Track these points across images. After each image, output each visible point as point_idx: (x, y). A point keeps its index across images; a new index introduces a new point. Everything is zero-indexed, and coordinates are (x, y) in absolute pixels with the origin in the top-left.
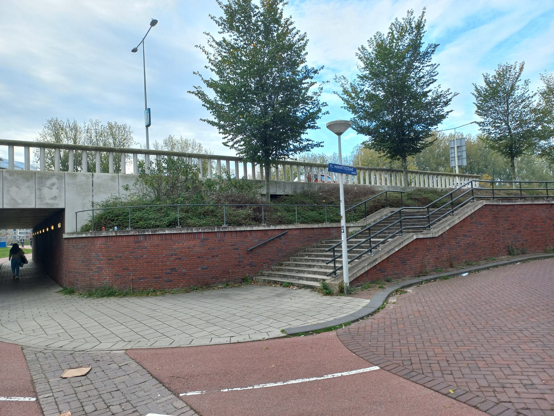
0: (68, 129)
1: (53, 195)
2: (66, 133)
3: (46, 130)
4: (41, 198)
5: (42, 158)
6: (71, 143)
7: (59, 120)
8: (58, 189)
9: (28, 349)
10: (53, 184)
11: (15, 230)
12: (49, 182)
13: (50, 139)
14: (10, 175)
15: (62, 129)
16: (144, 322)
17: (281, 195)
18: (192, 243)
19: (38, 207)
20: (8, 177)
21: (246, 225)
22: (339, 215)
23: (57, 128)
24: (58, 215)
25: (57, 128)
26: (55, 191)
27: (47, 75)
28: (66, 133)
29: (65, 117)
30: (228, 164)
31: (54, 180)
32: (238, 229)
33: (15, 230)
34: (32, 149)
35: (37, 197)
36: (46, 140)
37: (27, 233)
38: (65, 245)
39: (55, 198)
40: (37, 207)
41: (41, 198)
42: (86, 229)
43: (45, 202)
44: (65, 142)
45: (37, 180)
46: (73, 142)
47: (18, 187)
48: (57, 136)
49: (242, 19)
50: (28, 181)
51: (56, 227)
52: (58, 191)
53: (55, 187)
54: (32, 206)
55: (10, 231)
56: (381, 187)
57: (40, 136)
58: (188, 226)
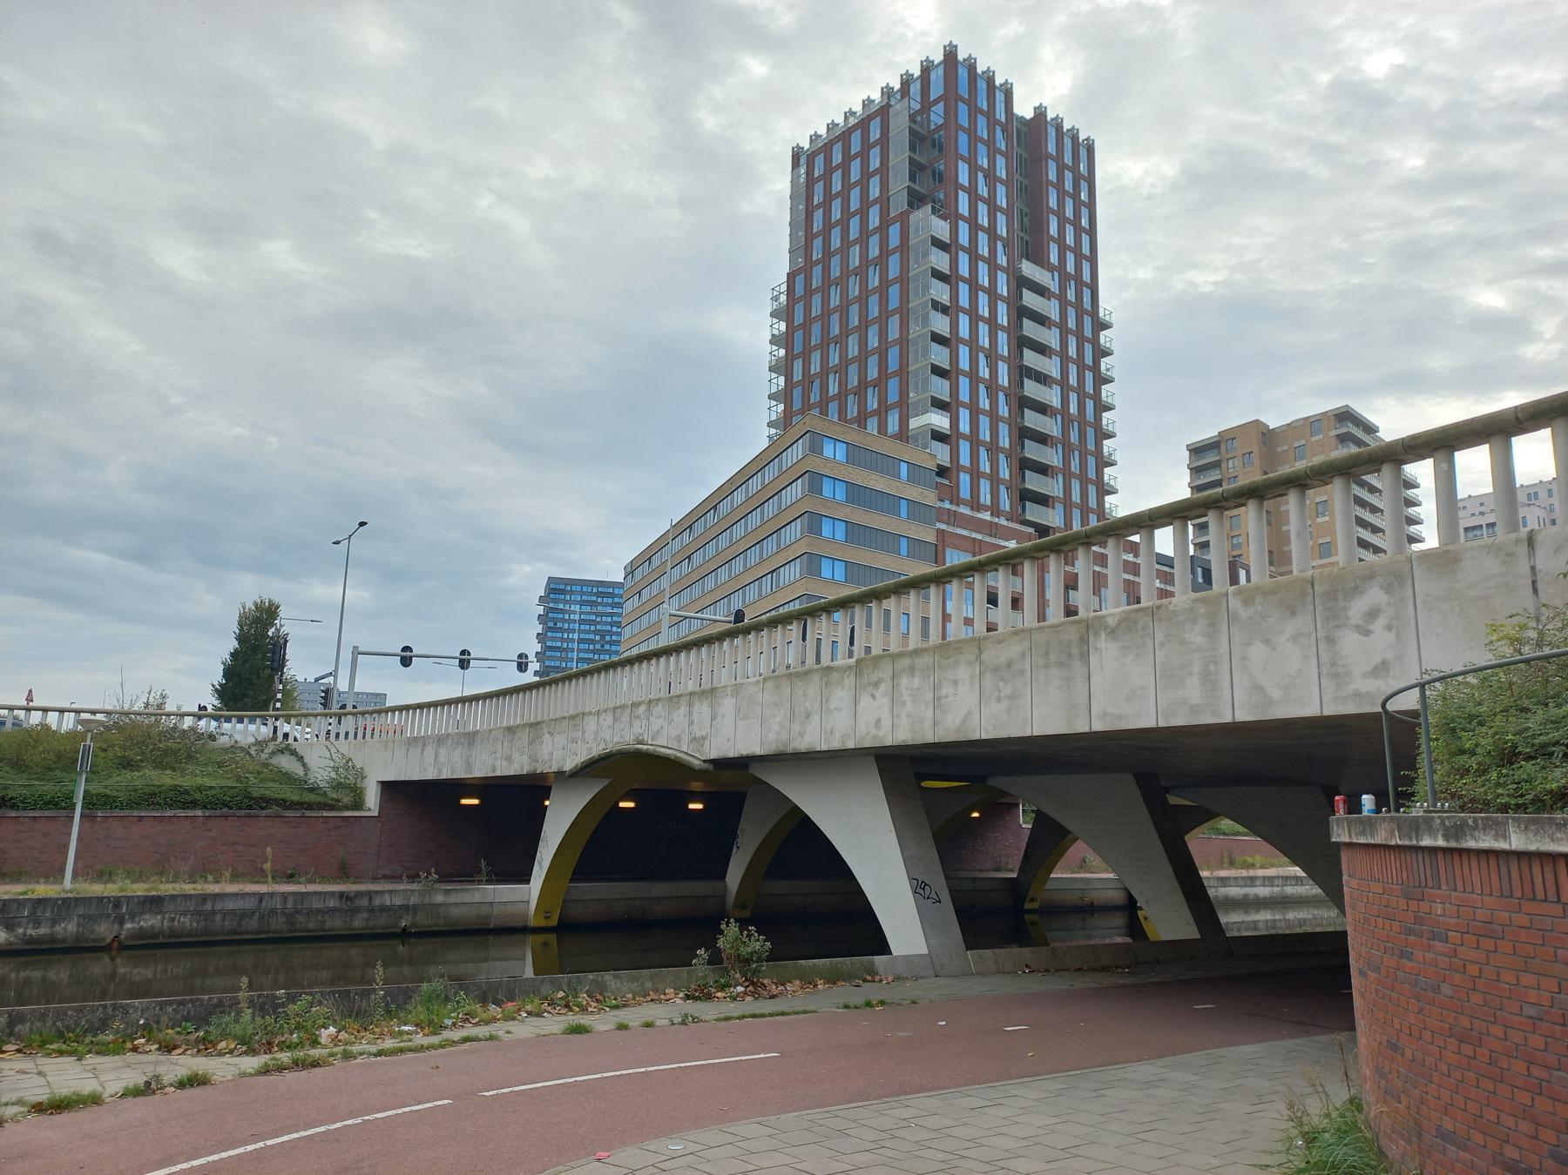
1: (1377, 660)
4: (1336, 675)
8: (1389, 628)
10: (1373, 614)
12: (1358, 607)
35: (1324, 671)
41: (1338, 675)
43: (1350, 689)
45: (1319, 608)
47: (1267, 642)
50: (1293, 614)
53: (1382, 621)
54: (1311, 710)
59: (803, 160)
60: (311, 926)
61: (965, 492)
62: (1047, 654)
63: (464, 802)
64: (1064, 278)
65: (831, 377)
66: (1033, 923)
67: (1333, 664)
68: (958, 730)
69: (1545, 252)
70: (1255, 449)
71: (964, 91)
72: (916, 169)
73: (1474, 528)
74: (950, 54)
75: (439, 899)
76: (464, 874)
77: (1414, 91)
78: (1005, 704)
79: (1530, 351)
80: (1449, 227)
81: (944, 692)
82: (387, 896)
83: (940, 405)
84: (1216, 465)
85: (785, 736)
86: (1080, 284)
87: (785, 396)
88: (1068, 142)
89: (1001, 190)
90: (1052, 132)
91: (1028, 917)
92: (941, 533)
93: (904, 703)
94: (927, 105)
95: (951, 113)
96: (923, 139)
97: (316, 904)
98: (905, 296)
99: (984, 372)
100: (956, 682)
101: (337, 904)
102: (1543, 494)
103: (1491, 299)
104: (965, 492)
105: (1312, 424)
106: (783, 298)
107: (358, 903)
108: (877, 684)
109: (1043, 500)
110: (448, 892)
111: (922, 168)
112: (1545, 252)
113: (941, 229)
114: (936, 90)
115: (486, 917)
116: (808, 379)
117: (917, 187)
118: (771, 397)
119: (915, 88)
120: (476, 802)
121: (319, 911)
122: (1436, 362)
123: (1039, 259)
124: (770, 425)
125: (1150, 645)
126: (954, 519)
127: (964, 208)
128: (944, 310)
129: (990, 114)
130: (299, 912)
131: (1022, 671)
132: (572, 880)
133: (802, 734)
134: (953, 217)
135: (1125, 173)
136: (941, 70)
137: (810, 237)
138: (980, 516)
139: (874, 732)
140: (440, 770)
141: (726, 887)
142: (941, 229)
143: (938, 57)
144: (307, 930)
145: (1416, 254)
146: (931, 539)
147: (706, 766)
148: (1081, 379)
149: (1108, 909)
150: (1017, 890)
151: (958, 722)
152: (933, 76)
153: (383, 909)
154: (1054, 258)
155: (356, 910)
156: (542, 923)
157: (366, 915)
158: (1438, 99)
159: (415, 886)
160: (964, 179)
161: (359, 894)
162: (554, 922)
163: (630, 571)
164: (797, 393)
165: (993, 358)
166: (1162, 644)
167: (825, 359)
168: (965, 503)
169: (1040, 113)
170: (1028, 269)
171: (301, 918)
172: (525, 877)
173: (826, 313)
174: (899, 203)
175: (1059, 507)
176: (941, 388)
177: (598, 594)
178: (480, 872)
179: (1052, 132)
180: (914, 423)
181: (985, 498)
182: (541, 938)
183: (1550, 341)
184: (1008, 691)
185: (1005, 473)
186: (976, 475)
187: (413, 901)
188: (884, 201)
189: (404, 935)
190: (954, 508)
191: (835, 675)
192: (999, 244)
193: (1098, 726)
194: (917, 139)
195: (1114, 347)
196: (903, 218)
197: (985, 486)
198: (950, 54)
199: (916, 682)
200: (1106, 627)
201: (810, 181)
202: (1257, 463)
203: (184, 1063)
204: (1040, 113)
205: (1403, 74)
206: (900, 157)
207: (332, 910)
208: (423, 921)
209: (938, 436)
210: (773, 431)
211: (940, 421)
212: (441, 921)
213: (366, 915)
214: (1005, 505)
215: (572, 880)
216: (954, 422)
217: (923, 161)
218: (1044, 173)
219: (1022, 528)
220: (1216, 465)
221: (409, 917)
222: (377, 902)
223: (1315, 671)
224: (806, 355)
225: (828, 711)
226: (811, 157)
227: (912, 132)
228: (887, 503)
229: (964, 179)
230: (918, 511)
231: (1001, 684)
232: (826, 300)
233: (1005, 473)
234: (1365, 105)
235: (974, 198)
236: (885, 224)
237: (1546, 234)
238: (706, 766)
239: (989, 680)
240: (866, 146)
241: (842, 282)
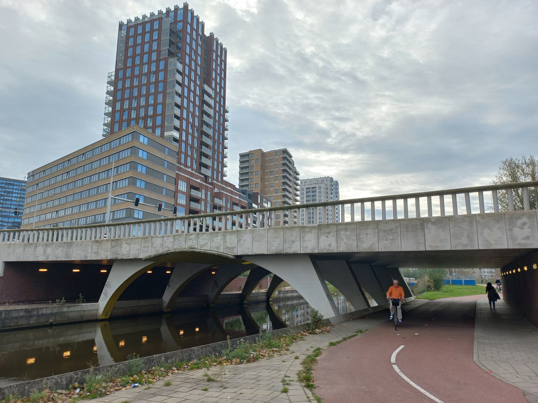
0: (524, 166)
1: (526, 235)
2: (523, 170)
3: (502, 171)
4: (513, 239)
5: (496, 199)
6: (529, 180)
7: (514, 159)
8: (529, 228)
9: (531, 396)
10: (524, 224)
11: (480, 269)
12: (519, 222)
13: (506, 179)
14: (482, 218)
15: (518, 167)
16: (513, 365)
19: (63, 260)
20: (481, 221)
23: (512, 167)
25: (512, 167)
26: (527, 231)
27: (493, 119)
28: (523, 170)
29: (519, 153)
31: (525, 219)
33: (480, 269)
34: (485, 193)
35: (509, 237)
36: (502, 181)
37: (491, 272)
39: (528, 238)
40: (510, 248)
41: (513, 239)
43: (518, 242)
44: (523, 179)
45: (507, 222)
46: (531, 178)
47: (490, 229)
48: (513, 175)
50: (498, 222)
52: (530, 230)
53: (527, 226)
54: (505, 247)
55: (476, 270)
57: (496, 178)
59: (124, 28)
60: (12, 324)
61: (183, 161)
62: (407, 228)
63: (74, 271)
64: (216, 93)
65: (133, 111)
66: (246, 308)
67: (511, 236)
68: (368, 248)
69: (337, 114)
70: (260, 158)
71: (189, 20)
72: (171, 43)
73: (308, 188)
74: (186, 6)
75: (65, 310)
76: (72, 299)
77: (316, 61)
78: (389, 242)
79: (329, 140)
80: (317, 102)
81: (362, 237)
82: (45, 310)
83: (176, 129)
84: (248, 161)
85: (281, 248)
86: (220, 96)
87: (112, 115)
88: (219, 47)
89: (199, 58)
90: (215, 42)
91: (245, 306)
92: (177, 174)
93: (343, 239)
94: (176, 22)
95: (185, 27)
96: (174, 33)
97: (15, 315)
98: (165, 88)
99: (191, 120)
100: (367, 234)
101: (24, 314)
102: (325, 181)
103: (322, 124)
104: (183, 161)
105: (276, 152)
106: (113, 78)
107: (32, 313)
108: (329, 233)
109: (206, 167)
110: (69, 307)
111: (173, 44)
112: (337, 114)
113: (180, 67)
114: (180, 17)
115: (82, 316)
116: (122, 111)
117: (171, 49)
118: (105, 114)
119: (172, 15)
120: (46, 270)
121: (16, 318)
122: (307, 140)
123: (210, 85)
124: (104, 125)
125: (448, 227)
126: (180, 169)
127: (187, 62)
128: (180, 96)
129: (197, 31)
130: (7, 319)
131: (397, 232)
132: (118, 300)
133: (290, 248)
134: (183, 63)
135: (234, 62)
136: (182, 11)
137: (126, 57)
138: (188, 169)
139: (328, 248)
140: (48, 257)
141: (163, 300)
142: (180, 67)
143: (181, 6)
144: (10, 326)
145: (308, 108)
146: (174, 176)
147: (234, 257)
148: (219, 128)
149: (262, 302)
150: (242, 297)
151: (368, 246)
152: (179, 12)
153: (43, 315)
154: (213, 86)
155: (32, 316)
156: (104, 317)
157: (36, 318)
158: (321, 64)
159: (55, 305)
160: (188, 51)
161: (33, 310)
162: (108, 317)
163: (32, 175)
164: (117, 115)
165: (193, 115)
166: (452, 228)
167: (130, 104)
168: (182, 164)
169: (212, 35)
170: (206, 87)
171: (8, 321)
172: (96, 299)
173: (132, 87)
174: (164, 53)
175: (211, 169)
176: (177, 123)
177: (6, 184)
178: (79, 298)
179: (215, 42)
180: (166, 134)
181: (189, 164)
182: (103, 323)
183: (333, 139)
184: (391, 237)
185: (195, 156)
186: (186, 156)
187: (55, 311)
188: (159, 52)
189: (51, 325)
190: (179, 165)
191: (307, 229)
192: (198, 77)
193: (428, 249)
194: (172, 33)
195: (229, 119)
196: (166, 60)
197: (189, 160)
198: (186, 6)
199: (348, 233)
200: (431, 221)
201: (128, 37)
202: (260, 162)
203: (213, 370)
204: (212, 35)
205: (315, 55)
206: (166, 38)
207: (22, 317)
208: (59, 319)
209: (175, 140)
210: (105, 127)
211: (176, 134)
212: (66, 319)
213: (36, 318)
214: (195, 167)
215: (118, 300)
216: (181, 136)
217: (174, 41)
218: (211, 55)
219: (200, 175)
220: (248, 161)
221: (53, 318)
222: (40, 312)
223: (506, 237)
224: (122, 100)
225: (304, 240)
226: (129, 28)
227: (171, 30)
228: (161, 162)
229: (188, 51)
230: (171, 166)
231: (388, 236)
232: (132, 82)
233: (195, 156)
234: (305, 61)
235: (191, 59)
236: (158, 61)
237: (338, 109)
238: (234, 257)
239: (381, 234)
240: (152, 31)
241: (139, 76)
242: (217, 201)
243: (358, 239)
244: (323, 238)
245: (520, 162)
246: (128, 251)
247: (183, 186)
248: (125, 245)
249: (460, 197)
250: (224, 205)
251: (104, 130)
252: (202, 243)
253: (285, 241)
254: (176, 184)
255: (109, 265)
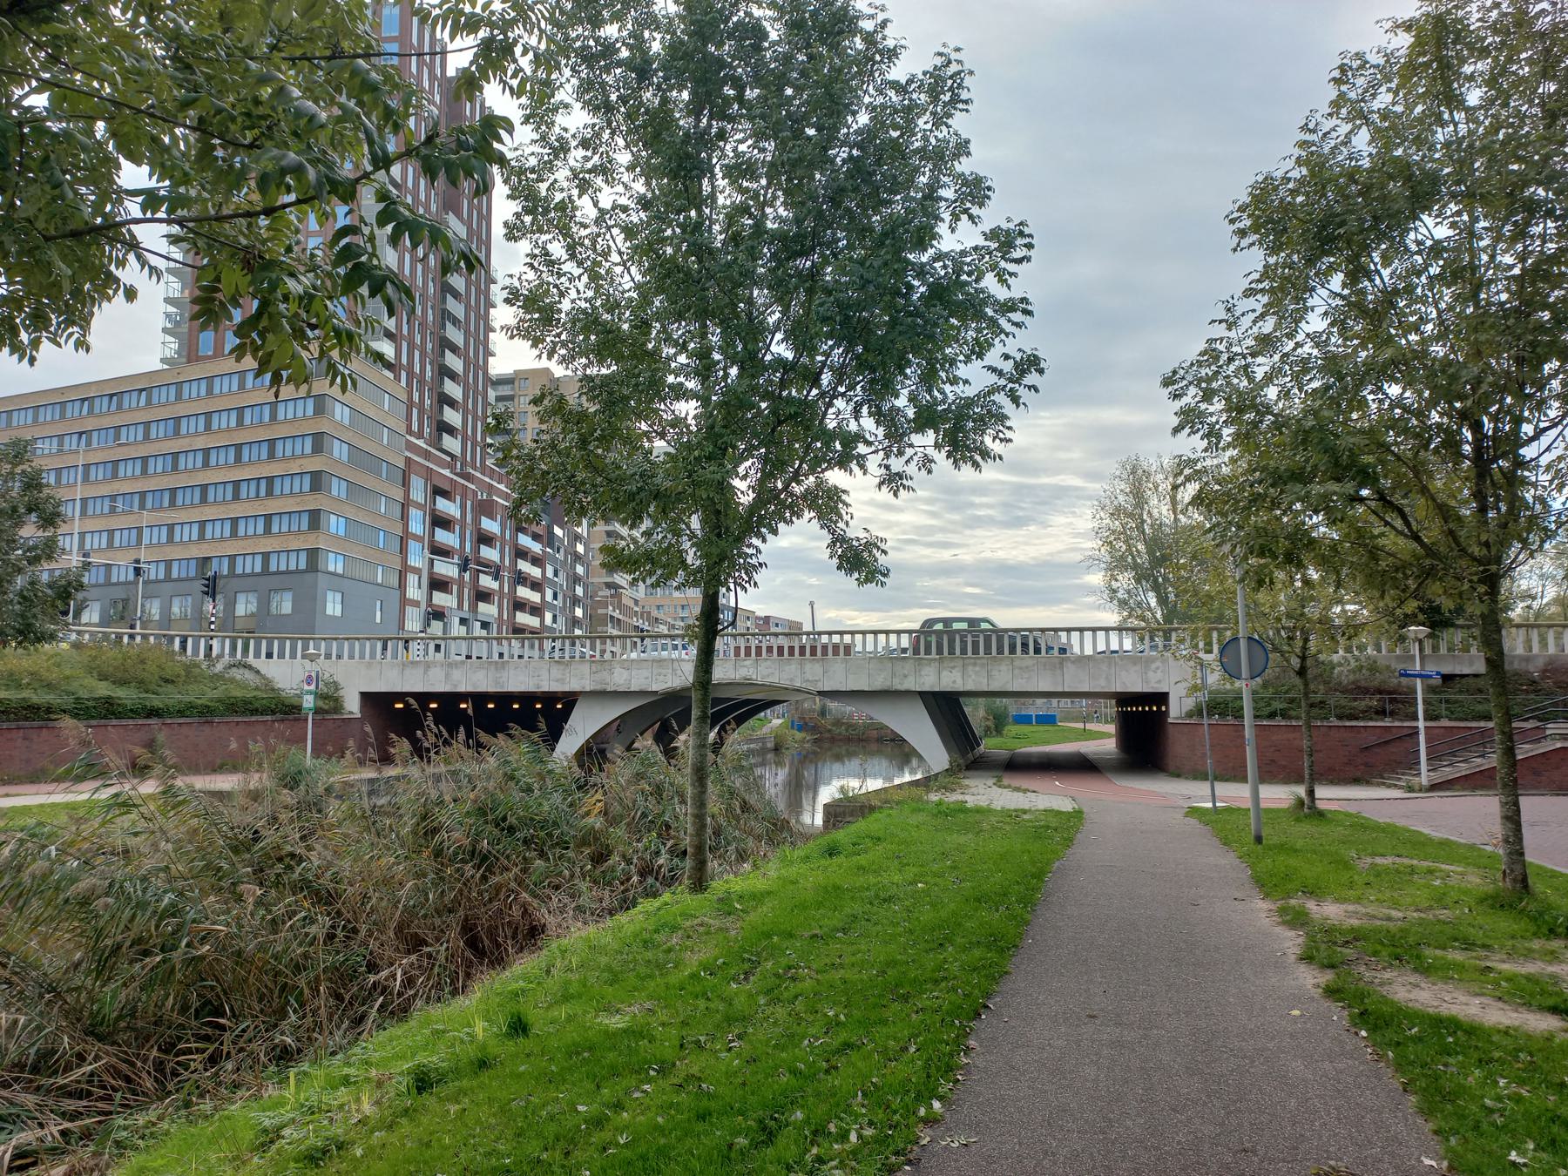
12: (1153, 666)
17: (1463, 676)
18: (1291, 736)
19: (490, 690)
21: (1363, 719)
22: (1416, 713)
24: (1162, 698)
26: (1159, 675)
30: (1069, 639)
31: (1158, 664)
32: (1348, 724)
38: (1171, 730)
42: (1190, 715)
49: (860, 349)
51: (1159, 708)
56: (1527, 659)
58: (1290, 718)
83: (389, 335)
92: (408, 460)
124: (168, 300)
210: (171, 309)
242: (443, 505)
243: (989, 676)
244: (945, 673)
245: (1154, 468)
246: (620, 679)
247: (418, 492)
248: (618, 670)
249: (1101, 634)
250: (458, 515)
251: (168, 315)
252: (765, 672)
253: (893, 675)
254: (406, 483)
255: (570, 700)
